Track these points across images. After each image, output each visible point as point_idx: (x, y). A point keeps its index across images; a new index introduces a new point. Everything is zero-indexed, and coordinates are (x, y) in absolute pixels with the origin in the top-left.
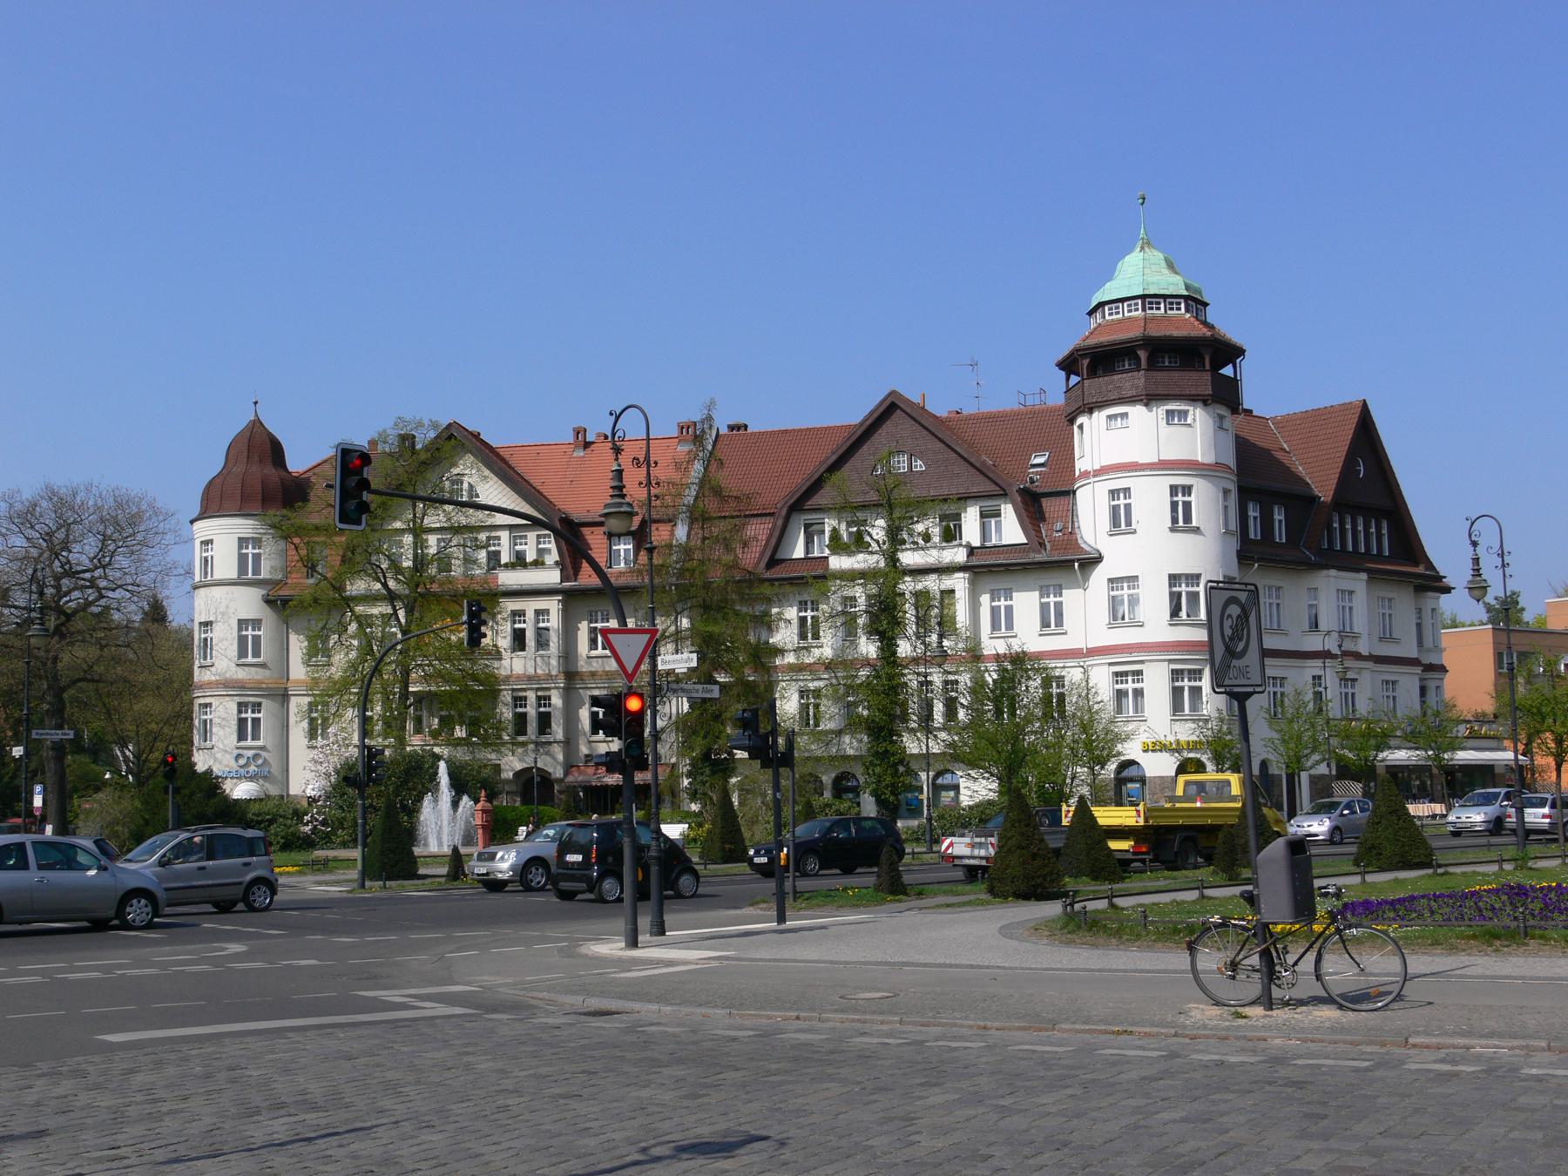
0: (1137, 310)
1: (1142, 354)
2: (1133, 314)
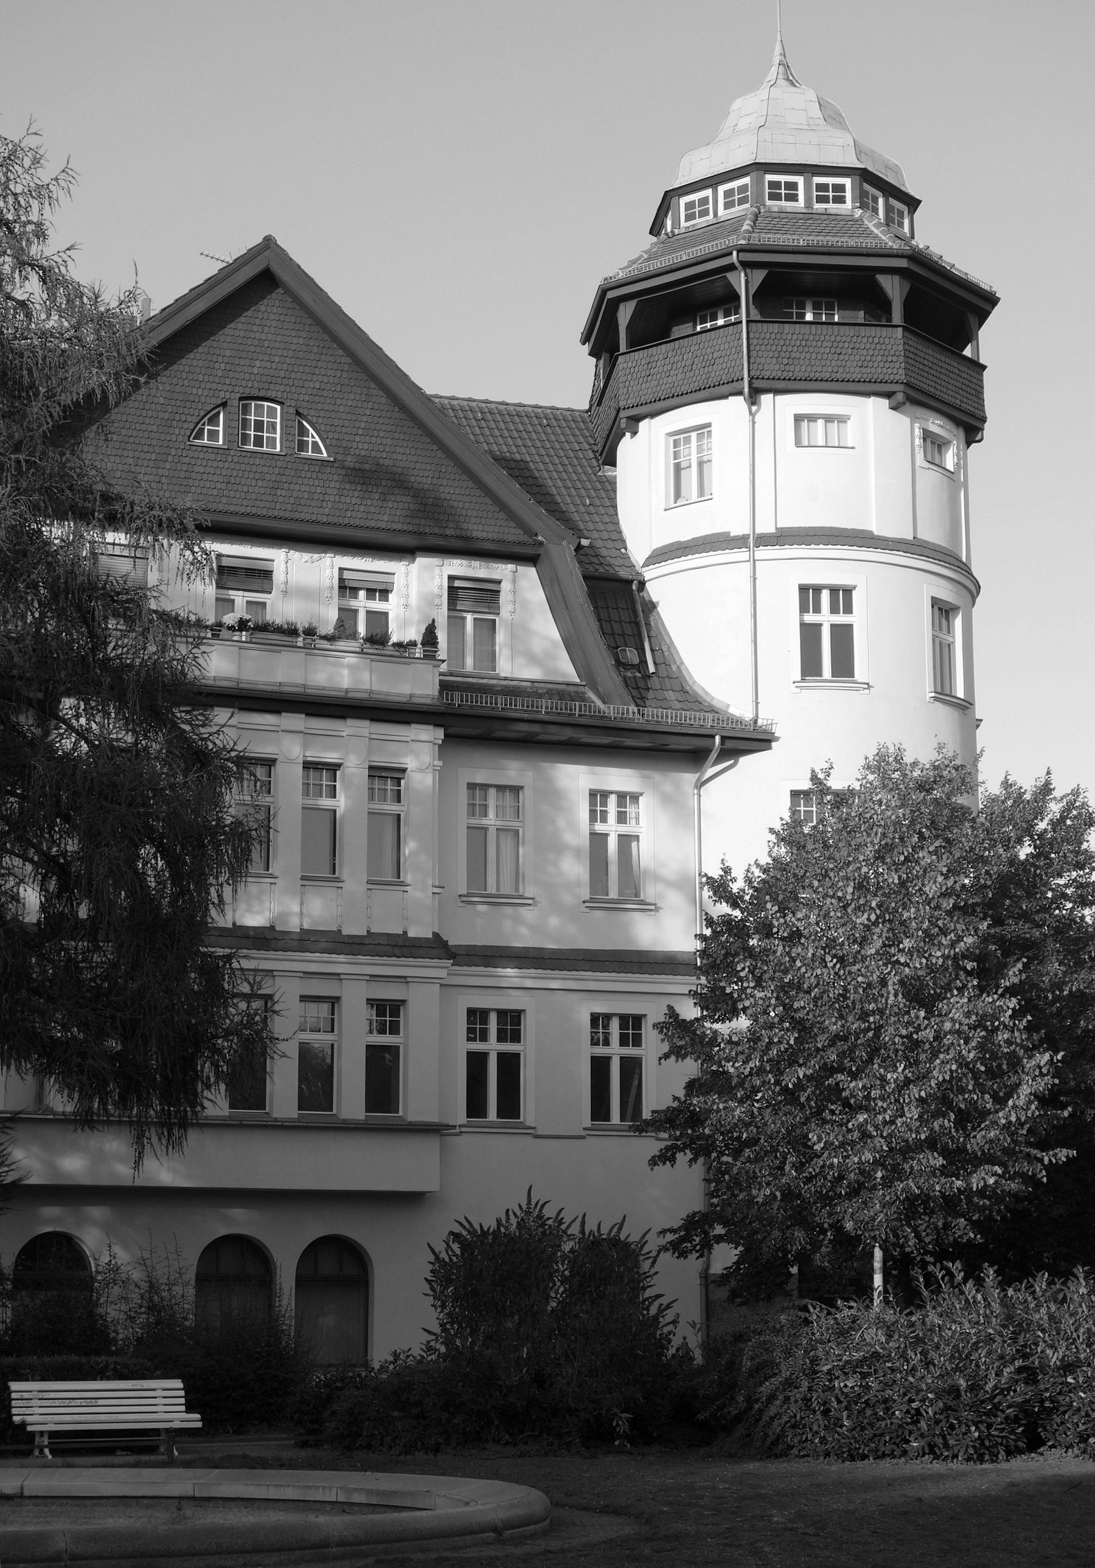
0: (840, 200)
1: (893, 288)
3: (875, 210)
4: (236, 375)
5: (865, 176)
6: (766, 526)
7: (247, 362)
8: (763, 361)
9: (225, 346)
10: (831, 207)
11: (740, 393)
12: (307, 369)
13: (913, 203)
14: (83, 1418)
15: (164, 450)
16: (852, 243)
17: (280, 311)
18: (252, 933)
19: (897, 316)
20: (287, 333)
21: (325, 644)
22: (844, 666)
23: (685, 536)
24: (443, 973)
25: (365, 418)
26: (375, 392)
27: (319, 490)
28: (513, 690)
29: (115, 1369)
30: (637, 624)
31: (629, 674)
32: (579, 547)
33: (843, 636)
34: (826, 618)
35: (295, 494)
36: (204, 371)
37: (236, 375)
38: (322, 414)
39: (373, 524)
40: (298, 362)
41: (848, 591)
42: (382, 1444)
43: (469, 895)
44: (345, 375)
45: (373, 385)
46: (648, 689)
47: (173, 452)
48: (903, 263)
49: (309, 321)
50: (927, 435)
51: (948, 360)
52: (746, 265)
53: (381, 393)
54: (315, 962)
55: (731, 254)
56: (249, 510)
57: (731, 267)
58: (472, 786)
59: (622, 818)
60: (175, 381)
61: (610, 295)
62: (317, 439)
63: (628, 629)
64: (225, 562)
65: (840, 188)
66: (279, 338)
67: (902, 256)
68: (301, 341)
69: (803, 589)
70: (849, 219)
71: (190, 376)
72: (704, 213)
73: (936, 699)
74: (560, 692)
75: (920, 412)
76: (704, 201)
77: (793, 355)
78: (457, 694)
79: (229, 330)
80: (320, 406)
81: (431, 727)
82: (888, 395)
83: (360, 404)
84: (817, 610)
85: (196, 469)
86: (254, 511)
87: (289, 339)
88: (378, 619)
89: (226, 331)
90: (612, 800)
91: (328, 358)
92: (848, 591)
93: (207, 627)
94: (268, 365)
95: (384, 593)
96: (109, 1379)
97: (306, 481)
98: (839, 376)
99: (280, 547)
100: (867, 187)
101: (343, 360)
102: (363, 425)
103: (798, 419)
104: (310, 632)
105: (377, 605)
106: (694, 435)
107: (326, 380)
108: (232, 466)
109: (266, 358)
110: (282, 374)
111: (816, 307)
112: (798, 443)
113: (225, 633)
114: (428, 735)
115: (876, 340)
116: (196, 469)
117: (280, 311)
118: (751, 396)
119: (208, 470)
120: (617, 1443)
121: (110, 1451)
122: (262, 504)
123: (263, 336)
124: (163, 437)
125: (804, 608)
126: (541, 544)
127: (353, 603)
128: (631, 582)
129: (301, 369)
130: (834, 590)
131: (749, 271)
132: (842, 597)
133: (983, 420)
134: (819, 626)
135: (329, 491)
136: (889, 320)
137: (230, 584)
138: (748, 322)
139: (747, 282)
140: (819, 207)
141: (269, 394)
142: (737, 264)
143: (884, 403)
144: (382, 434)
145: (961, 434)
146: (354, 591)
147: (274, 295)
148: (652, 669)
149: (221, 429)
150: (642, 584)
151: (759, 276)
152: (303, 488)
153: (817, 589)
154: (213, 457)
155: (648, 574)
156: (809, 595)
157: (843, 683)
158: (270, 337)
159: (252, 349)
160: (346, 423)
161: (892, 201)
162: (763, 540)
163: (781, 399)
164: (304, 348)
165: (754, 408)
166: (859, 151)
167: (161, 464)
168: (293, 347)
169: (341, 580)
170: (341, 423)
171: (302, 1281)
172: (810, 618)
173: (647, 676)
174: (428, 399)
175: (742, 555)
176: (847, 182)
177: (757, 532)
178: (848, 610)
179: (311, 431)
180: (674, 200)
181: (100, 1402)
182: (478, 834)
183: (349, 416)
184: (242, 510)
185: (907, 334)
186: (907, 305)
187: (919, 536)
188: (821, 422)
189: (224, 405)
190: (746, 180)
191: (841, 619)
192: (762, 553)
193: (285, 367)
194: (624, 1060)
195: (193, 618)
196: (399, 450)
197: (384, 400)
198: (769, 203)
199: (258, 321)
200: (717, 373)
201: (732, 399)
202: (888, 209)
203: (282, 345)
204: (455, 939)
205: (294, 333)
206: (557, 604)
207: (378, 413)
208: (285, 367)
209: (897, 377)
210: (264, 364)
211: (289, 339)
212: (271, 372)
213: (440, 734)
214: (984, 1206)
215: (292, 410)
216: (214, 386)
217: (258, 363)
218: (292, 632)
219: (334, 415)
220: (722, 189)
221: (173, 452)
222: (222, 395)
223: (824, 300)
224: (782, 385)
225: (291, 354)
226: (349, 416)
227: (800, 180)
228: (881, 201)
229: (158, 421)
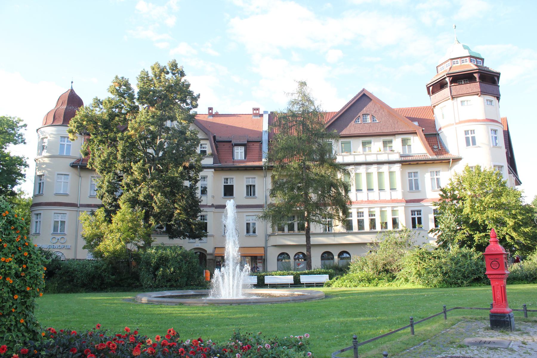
0: (467, 62)
1: (476, 75)
2: (465, 63)
5: (471, 57)
6: (457, 121)
10: (465, 63)
19: (478, 80)
22: (474, 143)
32: (423, 130)
33: (473, 139)
34: (470, 136)
41: (474, 131)
48: (477, 71)
57: (446, 78)
59: (415, 176)
63: (436, 142)
65: (466, 60)
69: (465, 131)
75: (485, 96)
82: (478, 94)
90: (413, 173)
92: (474, 131)
103: (462, 102)
121: (283, 287)
125: (466, 134)
130: (471, 131)
133: (500, 95)
136: (476, 81)
138: (450, 86)
153: (468, 131)
156: (466, 132)
162: (456, 124)
166: (470, 53)
174: (393, 109)
176: (468, 58)
178: (474, 133)
186: (480, 78)
194: (418, 218)
204: (215, 204)
213: (401, 164)
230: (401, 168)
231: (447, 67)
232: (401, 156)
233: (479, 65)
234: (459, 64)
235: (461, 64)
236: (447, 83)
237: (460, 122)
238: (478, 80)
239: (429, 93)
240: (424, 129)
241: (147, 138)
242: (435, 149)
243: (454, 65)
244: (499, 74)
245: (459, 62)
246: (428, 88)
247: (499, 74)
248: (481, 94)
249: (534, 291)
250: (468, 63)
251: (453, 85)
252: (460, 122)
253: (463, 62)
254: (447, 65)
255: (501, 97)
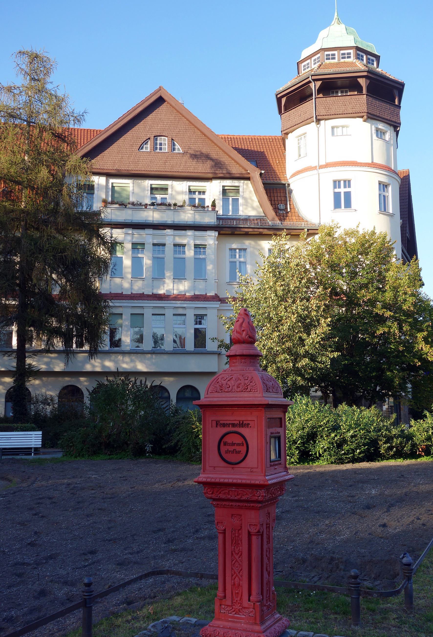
0: (349, 57)
1: (363, 82)
3: (363, 60)
4: (153, 129)
5: (358, 49)
6: (322, 163)
7: (156, 125)
8: (320, 110)
9: (149, 121)
10: (346, 60)
11: (313, 122)
12: (175, 126)
13: (378, 58)
14: (7, 444)
15: (131, 154)
16: (348, 69)
17: (166, 109)
18: (158, 296)
19: (364, 91)
20: (169, 115)
21: (179, 208)
22: (348, 204)
23: (299, 168)
24: (218, 306)
25: (193, 139)
26: (196, 131)
27: (179, 162)
28: (247, 219)
29: (20, 428)
30: (286, 197)
31: (281, 212)
32: (261, 174)
33: (348, 195)
34: (342, 190)
35: (172, 164)
36: (143, 129)
37: (153, 129)
38: (180, 139)
39: (196, 171)
40: (172, 124)
41: (349, 181)
42: (70, 454)
43: (229, 282)
44: (187, 126)
45: (196, 129)
46: (287, 216)
47: (134, 154)
48: (365, 74)
49: (175, 111)
50: (377, 130)
51: (385, 105)
52: (314, 80)
53: (198, 131)
54: (178, 304)
55: (309, 77)
56: (157, 170)
57: (310, 82)
58: (231, 249)
60: (134, 133)
61: (278, 96)
62: (179, 147)
63: (283, 199)
64: (153, 186)
65: (349, 54)
66: (166, 117)
67: (365, 71)
68: (173, 117)
69: (335, 182)
70: (352, 63)
71: (139, 131)
72: (308, 68)
73: (380, 213)
74: (260, 219)
76: (308, 64)
77: (330, 107)
78: (221, 221)
79: (150, 116)
80: (179, 137)
81: (214, 231)
82: (362, 117)
83: (192, 135)
84: (339, 187)
85: (141, 158)
86: (159, 170)
87: (169, 117)
88: (202, 201)
89: (149, 116)
91: (181, 122)
93: (143, 205)
94: (163, 125)
95: (204, 193)
96: (18, 431)
97: (175, 160)
98: (345, 112)
99: (170, 180)
100: (358, 52)
101: (186, 122)
102: (193, 141)
103: (333, 128)
104: (175, 205)
105: (202, 196)
106: (303, 137)
107: (181, 128)
108: (152, 157)
109: (162, 123)
110: (167, 128)
111: (342, 92)
112: (333, 134)
113: (148, 207)
114: (214, 234)
115: (357, 100)
116: (141, 158)
117: (166, 109)
118: (316, 122)
119: (144, 158)
120: (147, 455)
122: (161, 167)
123: (161, 117)
124: (130, 150)
125: (335, 187)
126: (249, 173)
127: (194, 196)
128: (285, 184)
129: (173, 126)
130: (345, 181)
131: (316, 82)
132: (348, 183)
133: (400, 124)
134: (340, 193)
135: (182, 162)
137: (155, 193)
138: (315, 98)
139: (315, 86)
140: (342, 60)
141: (163, 134)
142: (311, 80)
143: (361, 119)
144: (199, 144)
145: (392, 128)
146: (194, 192)
147: (164, 104)
148: (289, 210)
149: (149, 146)
150: (289, 185)
151: (319, 83)
152: (174, 162)
153: (339, 181)
154: (146, 154)
155: (290, 181)
156: (336, 183)
157: (348, 209)
158: (163, 117)
159: (158, 121)
160: (188, 141)
161: (369, 56)
162: (321, 167)
163: (327, 121)
164: (174, 119)
165: (318, 126)
167: (130, 158)
168: (170, 119)
169: (189, 189)
170: (186, 141)
171: (178, 399)
172: (337, 190)
173: (287, 212)
174: (218, 135)
175: (315, 172)
176: (351, 51)
177: (320, 164)
178: (349, 186)
179: (177, 145)
180: (300, 65)
181: (12, 439)
182: (233, 263)
183: (188, 139)
184: (155, 170)
185: (368, 97)
187: (374, 162)
188: (341, 128)
189: (149, 139)
190: (319, 55)
191: (347, 190)
192: (321, 171)
193: (168, 126)
195: (139, 203)
196: (204, 148)
197: (199, 133)
198: (326, 61)
199: (159, 113)
200: (307, 116)
201: (312, 123)
202: (368, 59)
203: (167, 119)
205: (170, 115)
206: (256, 191)
207: (197, 137)
208: (168, 126)
209: (364, 111)
210: (161, 125)
211: (169, 117)
212: (164, 128)
213: (217, 233)
214: (310, 373)
215: (170, 139)
216: (146, 133)
217: (159, 125)
218: (170, 205)
219: (183, 139)
220: (313, 59)
221: (134, 154)
222: (148, 136)
223: (344, 90)
224: (326, 117)
225: (170, 121)
226: (188, 139)
227: (336, 52)
228: (365, 57)
229: (129, 145)
230: (218, 239)
231: (315, 64)
232: (218, 219)
233: (370, 65)
234: (336, 61)
235: (339, 60)
236: (311, 95)
237: (327, 165)
238: (364, 91)
239: (280, 112)
240: (263, 172)
241: (309, 402)
242: (281, 210)
243: (327, 62)
244: (403, 85)
245: (336, 57)
246: (279, 100)
247: (403, 85)
248: (368, 117)
249: (414, 467)
250: (352, 59)
251: (321, 95)
252: (327, 165)
253: (343, 58)
254: (315, 60)
255: (402, 129)
